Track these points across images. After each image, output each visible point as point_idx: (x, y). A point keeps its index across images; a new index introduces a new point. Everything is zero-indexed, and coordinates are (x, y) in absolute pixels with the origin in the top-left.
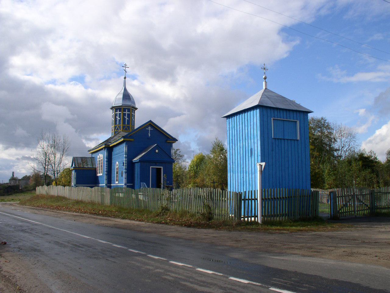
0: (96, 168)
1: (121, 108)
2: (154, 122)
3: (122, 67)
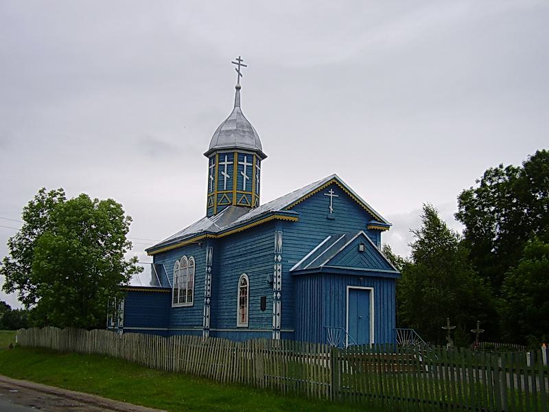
3: (233, 62)
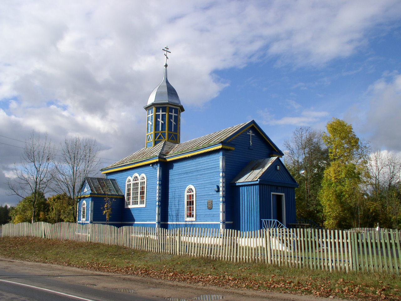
0: (124, 196)
2: (259, 125)
3: (163, 50)
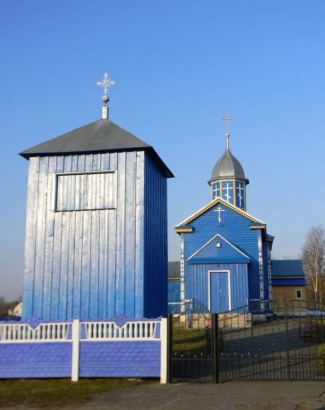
1: (219, 183)
